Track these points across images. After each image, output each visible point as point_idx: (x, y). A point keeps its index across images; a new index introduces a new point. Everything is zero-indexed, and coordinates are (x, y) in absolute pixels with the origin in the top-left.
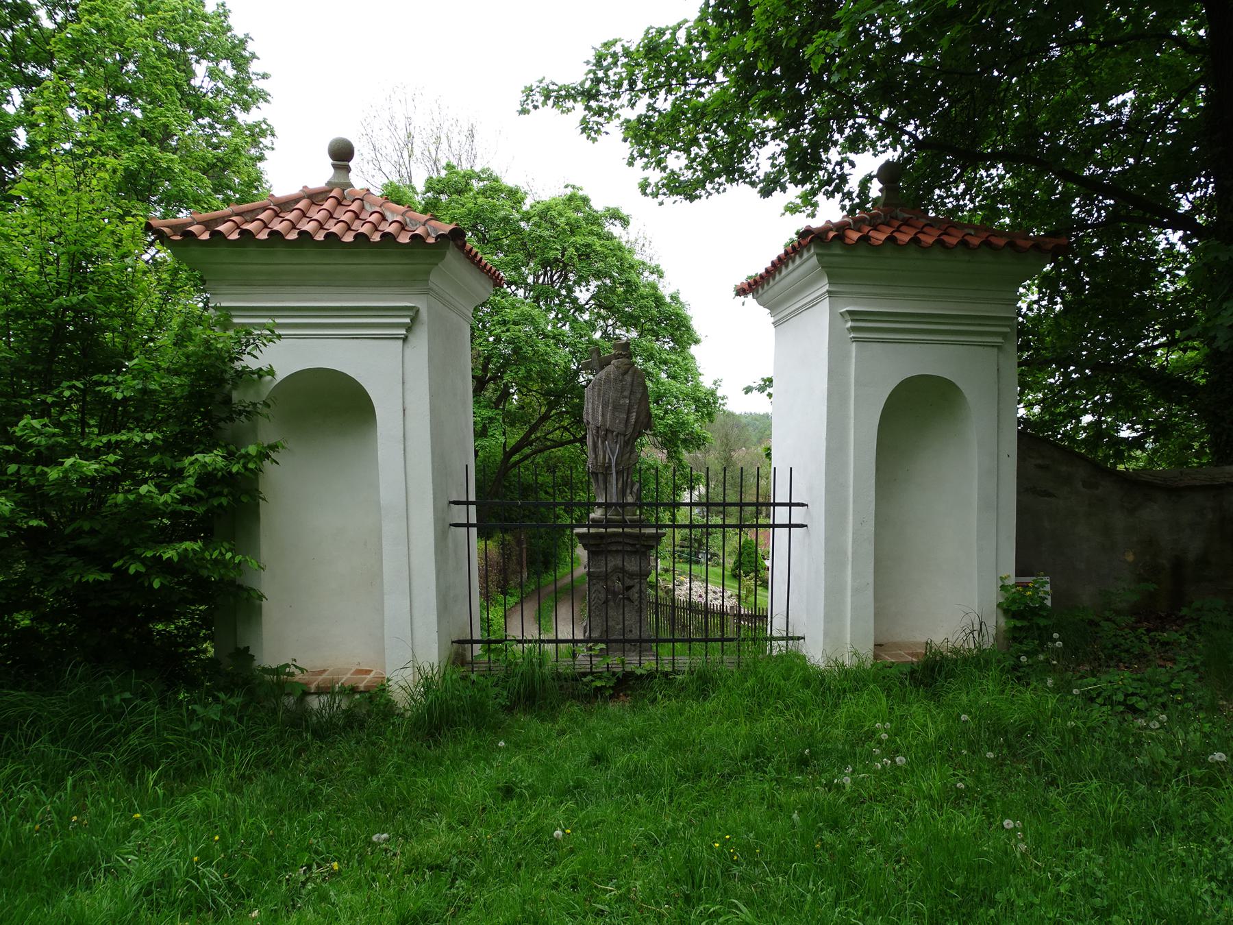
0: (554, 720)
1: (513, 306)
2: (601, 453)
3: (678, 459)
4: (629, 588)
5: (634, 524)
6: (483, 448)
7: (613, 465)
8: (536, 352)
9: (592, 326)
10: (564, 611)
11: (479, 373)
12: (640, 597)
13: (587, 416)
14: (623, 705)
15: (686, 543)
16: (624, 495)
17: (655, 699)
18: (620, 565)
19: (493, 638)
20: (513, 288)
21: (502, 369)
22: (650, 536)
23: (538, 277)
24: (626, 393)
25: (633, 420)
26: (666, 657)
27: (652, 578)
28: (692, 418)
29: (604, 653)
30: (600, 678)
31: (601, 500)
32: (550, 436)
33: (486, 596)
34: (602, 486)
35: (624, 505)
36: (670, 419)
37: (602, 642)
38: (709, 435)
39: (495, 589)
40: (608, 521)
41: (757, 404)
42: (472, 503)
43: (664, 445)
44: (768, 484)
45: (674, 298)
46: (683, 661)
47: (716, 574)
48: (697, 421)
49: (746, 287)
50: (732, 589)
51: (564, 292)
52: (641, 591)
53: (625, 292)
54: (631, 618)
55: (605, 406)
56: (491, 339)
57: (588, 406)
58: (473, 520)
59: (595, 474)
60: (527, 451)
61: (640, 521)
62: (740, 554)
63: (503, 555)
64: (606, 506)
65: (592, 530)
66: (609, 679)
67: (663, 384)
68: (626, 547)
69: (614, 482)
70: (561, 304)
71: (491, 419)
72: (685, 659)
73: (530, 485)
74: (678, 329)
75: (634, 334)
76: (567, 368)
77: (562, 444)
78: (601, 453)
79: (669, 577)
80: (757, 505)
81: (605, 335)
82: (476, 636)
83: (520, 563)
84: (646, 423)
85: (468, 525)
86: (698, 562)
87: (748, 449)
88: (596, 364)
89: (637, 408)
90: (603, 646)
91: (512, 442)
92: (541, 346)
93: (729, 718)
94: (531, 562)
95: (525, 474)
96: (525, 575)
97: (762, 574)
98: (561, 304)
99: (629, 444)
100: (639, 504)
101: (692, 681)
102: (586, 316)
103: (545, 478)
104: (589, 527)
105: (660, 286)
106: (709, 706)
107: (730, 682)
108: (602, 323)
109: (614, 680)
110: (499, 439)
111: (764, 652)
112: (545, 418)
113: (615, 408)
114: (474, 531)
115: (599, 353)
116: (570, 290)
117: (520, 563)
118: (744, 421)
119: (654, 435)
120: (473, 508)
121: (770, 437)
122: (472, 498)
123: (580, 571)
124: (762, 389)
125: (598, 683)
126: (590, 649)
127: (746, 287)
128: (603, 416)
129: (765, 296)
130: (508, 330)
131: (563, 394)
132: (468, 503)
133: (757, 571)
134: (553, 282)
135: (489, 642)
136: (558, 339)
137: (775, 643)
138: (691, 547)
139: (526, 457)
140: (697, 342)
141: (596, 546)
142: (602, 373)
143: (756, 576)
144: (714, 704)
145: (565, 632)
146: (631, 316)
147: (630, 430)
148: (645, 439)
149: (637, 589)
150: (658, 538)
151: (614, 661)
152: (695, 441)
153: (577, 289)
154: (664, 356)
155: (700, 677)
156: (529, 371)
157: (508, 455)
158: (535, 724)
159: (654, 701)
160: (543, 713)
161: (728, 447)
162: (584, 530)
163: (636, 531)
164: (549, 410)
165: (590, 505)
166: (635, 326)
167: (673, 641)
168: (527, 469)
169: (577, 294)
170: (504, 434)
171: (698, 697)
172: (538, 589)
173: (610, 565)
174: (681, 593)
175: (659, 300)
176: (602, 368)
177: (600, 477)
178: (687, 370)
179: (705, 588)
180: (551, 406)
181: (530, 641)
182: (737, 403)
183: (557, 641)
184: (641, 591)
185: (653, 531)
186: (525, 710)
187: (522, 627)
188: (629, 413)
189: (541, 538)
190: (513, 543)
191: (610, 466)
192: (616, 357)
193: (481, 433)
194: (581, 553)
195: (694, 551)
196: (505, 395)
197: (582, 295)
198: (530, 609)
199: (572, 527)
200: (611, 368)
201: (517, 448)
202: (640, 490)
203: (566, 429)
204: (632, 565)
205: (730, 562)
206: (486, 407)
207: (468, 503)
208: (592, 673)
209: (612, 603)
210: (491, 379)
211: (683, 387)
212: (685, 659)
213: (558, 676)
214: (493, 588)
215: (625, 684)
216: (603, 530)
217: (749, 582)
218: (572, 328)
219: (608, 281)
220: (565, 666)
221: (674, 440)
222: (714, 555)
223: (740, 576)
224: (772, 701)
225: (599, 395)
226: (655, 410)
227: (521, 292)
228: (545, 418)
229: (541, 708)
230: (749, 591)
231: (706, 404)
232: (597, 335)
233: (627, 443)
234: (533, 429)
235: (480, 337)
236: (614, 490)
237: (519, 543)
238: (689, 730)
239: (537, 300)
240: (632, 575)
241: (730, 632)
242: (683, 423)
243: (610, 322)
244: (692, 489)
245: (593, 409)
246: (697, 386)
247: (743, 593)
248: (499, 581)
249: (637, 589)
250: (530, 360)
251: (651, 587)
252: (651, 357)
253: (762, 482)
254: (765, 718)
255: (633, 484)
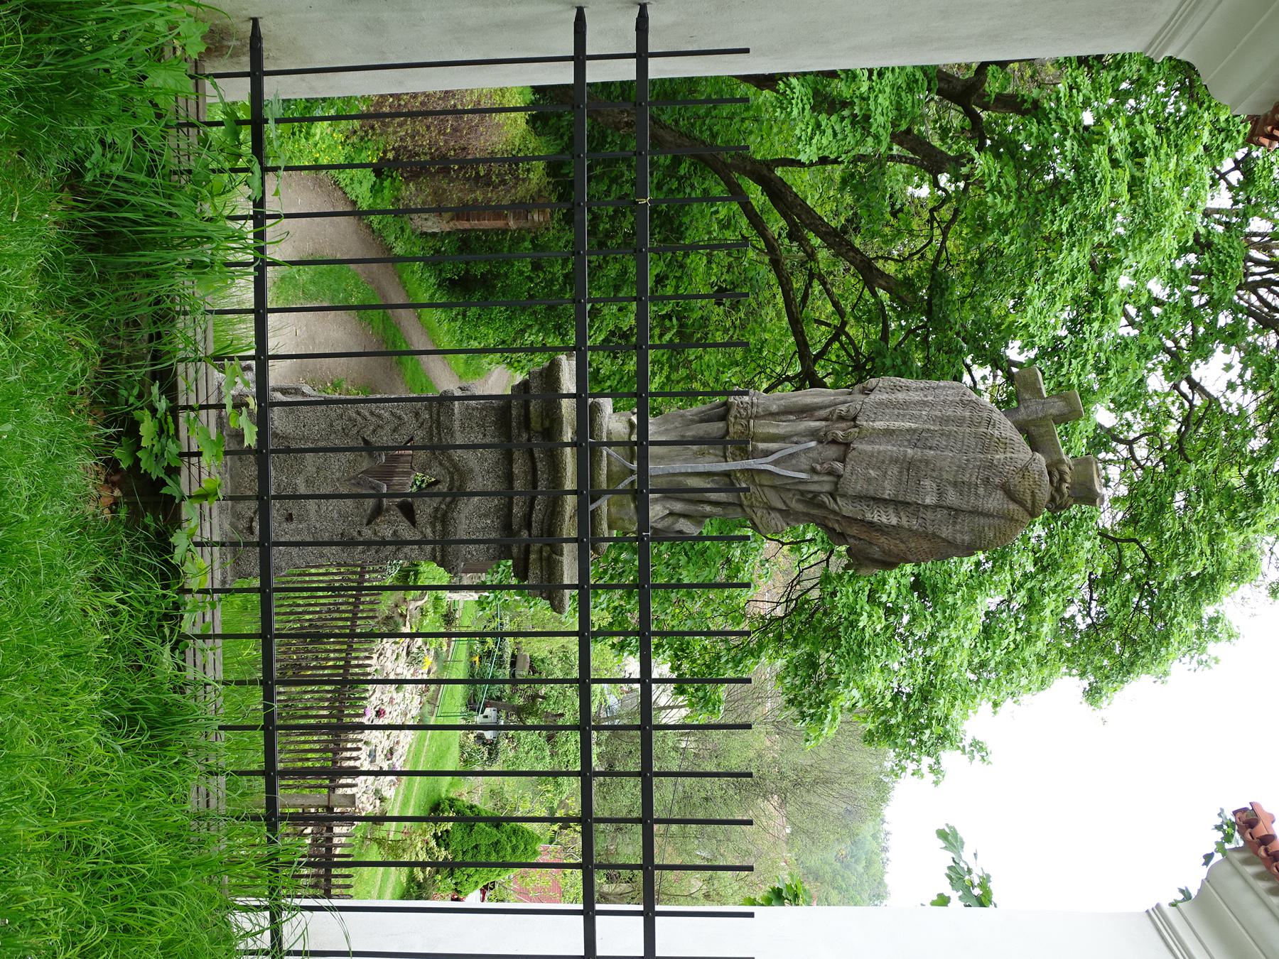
0: (47, 305)
1: (1184, 178)
2: (783, 428)
3: (761, 646)
4: (408, 511)
5: (586, 519)
6: (784, 102)
7: (751, 463)
8: (1053, 241)
9: (1132, 398)
10: (333, 332)
11: (993, 86)
12: (384, 543)
13: (884, 388)
14: (86, 498)
15: (523, 672)
16: (670, 492)
17: (107, 588)
18: (470, 487)
19: (271, 130)
20: (1235, 177)
21: (1006, 149)
22: (551, 567)
23: (1265, 248)
24: (952, 497)
25: (876, 516)
26: (222, 615)
27: (432, 573)
28: (876, 681)
29: (234, 449)
30: (161, 432)
31: (655, 429)
32: (817, 287)
33: (377, 115)
34: (690, 434)
35: (640, 496)
36: (871, 622)
37: (262, 435)
38: (829, 731)
39: (393, 141)
40: (595, 448)
41: (913, 866)
42: (642, 69)
43: (797, 605)
44: (691, 897)
45: (1211, 629)
46: (212, 663)
47: (442, 755)
48: (868, 693)
49: (1261, 830)
50: (401, 797)
51: (1224, 319)
52: (400, 543)
53: (1229, 493)
54: (323, 518)
55: (917, 438)
56: (1088, 118)
57: (912, 390)
58: (596, 73)
59: (723, 414)
60: (776, 224)
61: (597, 541)
62: (496, 822)
63: (490, 160)
64: (639, 446)
65: (568, 407)
66: (158, 457)
67: (970, 601)
68: (523, 503)
69: (701, 468)
70: (1189, 312)
71: (863, 123)
72: (216, 669)
73: (679, 232)
74: (1126, 639)
75: (1108, 517)
76: (1009, 332)
77: (796, 325)
78: (783, 428)
79: (432, 623)
80: (648, 866)
81: (1102, 439)
82: (271, 86)
83: (462, 212)
84: (870, 555)
85: (580, 58)
86: (472, 705)
87: (789, 840)
88: (1031, 410)
89: (891, 533)
90: (250, 439)
91: (802, 183)
92: (1073, 258)
93: (63, 792)
94: (465, 242)
95: (713, 219)
96: (433, 225)
97: (445, 883)
98: (1189, 312)
99: (816, 508)
100: (644, 539)
101: (155, 687)
102: (1157, 382)
103: (702, 273)
104: (579, 396)
105: (1245, 589)
106: (91, 737)
107: (156, 794)
108: (1138, 428)
109: (156, 472)
110: (804, 145)
111: (241, 889)
112: (868, 272)
113: (909, 465)
114: (563, 75)
115: (1061, 419)
116: (1232, 336)
117: (462, 212)
118: (866, 830)
119: (826, 579)
120: (626, 71)
121: (842, 903)
122: (658, 69)
123: (444, 377)
124: (957, 876)
125: (147, 428)
126: (239, 404)
127: (1261, 830)
128: (889, 432)
129: (1236, 883)
130: (1115, 163)
131: (932, 319)
132: (642, 56)
133: (450, 867)
134: (1253, 288)
135: (257, 122)
136: (1092, 303)
137: (264, 918)
138: (514, 681)
139: (757, 222)
140: (1093, 694)
141: (523, 422)
142: (1006, 428)
143: (437, 865)
144: (97, 750)
145: (285, 333)
146: (1160, 508)
147: (847, 508)
148: (813, 554)
149: (406, 532)
150: (551, 591)
151: (210, 471)
152: (810, 693)
153: (1235, 357)
154: (1050, 602)
155: (166, 710)
156: (1002, 224)
157: (763, 173)
158: (34, 253)
159: (101, 582)
160: (64, 275)
161: (795, 786)
162: (568, 383)
163: (569, 528)
164: (891, 284)
165: (639, 398)
166: (1133, 520)
167: (266, 635)
168: (726, 225)
169: (1220, 357)
170: (824, 161)
171: (115, 707)
172: (390, 259)
173: (470, 459)
174: (388, 658)
175: (1204, 585)
176: (1022, 428)
177: (716, 428)
178: (1010, 666)
179: (405, 729)
180: (902, 289)
181: (260, 236)
182: (915, 807)
183: (260, 312)
184: (400, 543)
185: (569, 573)
186: (72, 224)
187: (299, 218)
188: (898, 504)
189: (537, 267)
190: (521, 192)
191: (746, 455)
192: (1054, 467)
193: (827, 94)
194: (499, 379)
195: (502, 693)
196: (931, 162)
197: (1217, 372)
198: (338, 237)
199: (579, 351)
200: (1023, 452)
201: (780, 195)
202: (681, 537)
203: (839, 331)
204: (472, 518)
205: (474, 793)
206: (899, 107)
207: (642, 56)
208: (174, 410)
209: (365, 464)
210: (975, 119)
211: (961, 657)
212: (216, 669)
213: (164, 317)
214: (395, 136)
215: (146, 502)
216: (568, 435)
217: (419, 844)
218: (1122, 346)
219: (1256, 444)
220: (189, 334)
221: (811, 629)
222: (493, 747)
223: (437, 820)
224: (106, 911)
225: (945, 420)
226: (896, 581)
227: (1223, 199)
228: (868, 272)
229: (79, 268)
230: (395, 847)
231: (915, 722)
232: (1104, 416)
233: (812, 500)
234: (837, 240)
235: (1096, 87)
236: (679, 467)
237: (521, 208)
238: (23, 681)
239: (1203, 244)
240: (443, 519)
241: (291, 798)
242: (861, 658)
243: (1141, 452)
244: (680, 683)
245: (906, 405)
246: (966, 694)
247: (391, 830)
248: (415, 152)
249: (406, 532)
250: (1032, 228)
251: (404, 574)
252: (1045, 565)
253: (695, 882)
254: (59, 893)
255: (698, 519)
